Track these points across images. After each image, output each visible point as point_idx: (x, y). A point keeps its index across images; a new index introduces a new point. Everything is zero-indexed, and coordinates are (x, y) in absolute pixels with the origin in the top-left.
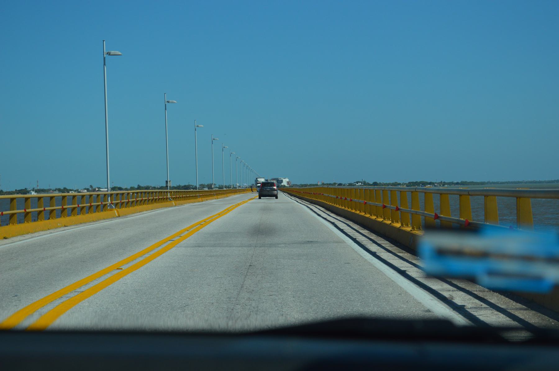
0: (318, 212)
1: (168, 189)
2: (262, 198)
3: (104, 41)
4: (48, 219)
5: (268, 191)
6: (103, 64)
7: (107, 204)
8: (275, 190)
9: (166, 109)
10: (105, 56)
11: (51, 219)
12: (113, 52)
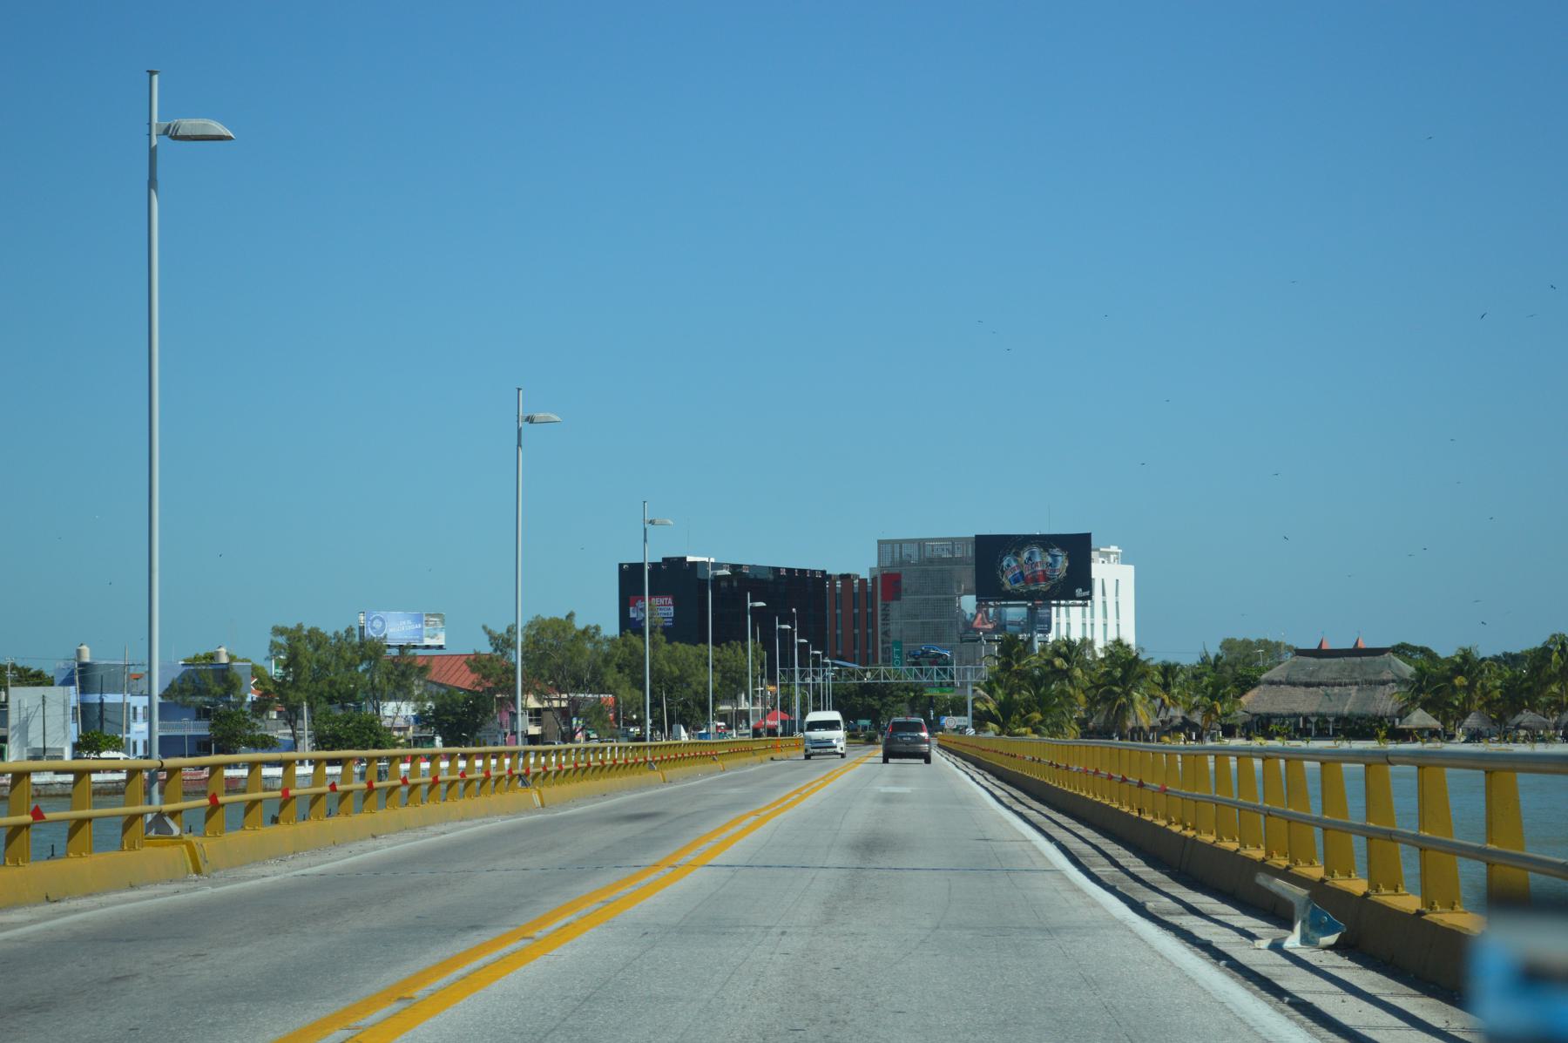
0: (1103, 848)
1: (517, 744)
2: (890, 760)
3: (519, 389)
4: (48, 858)
5: (907, 743)
6: (516, 444)
7: (142, 815)
8: (923, 741)
9: (519, 445)
10: (155, 142)
11: (282, 823)
12: (541, 415)
